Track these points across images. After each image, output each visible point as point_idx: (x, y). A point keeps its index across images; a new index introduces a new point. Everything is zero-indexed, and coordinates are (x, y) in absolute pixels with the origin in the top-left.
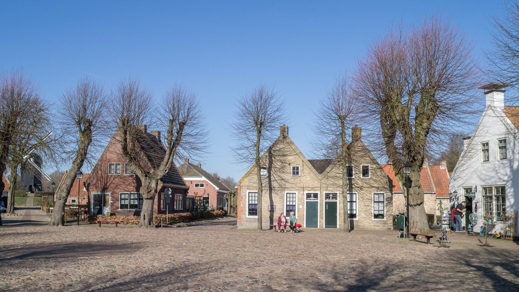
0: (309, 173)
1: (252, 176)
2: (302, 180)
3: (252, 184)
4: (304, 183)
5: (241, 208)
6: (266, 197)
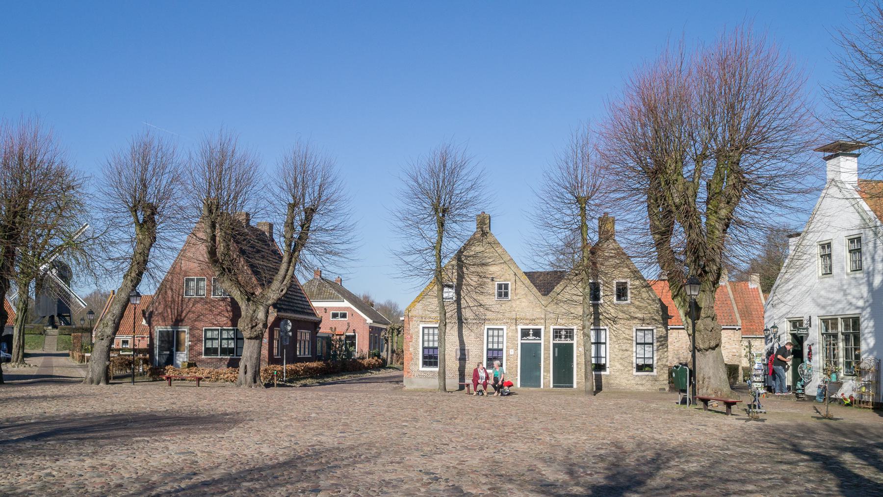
0: (525, 294)
1: (429, 300)
2: (514, 306)
3: (428, 312)
4: (518, 311)
5: (411, 354)
6: (453, 335)
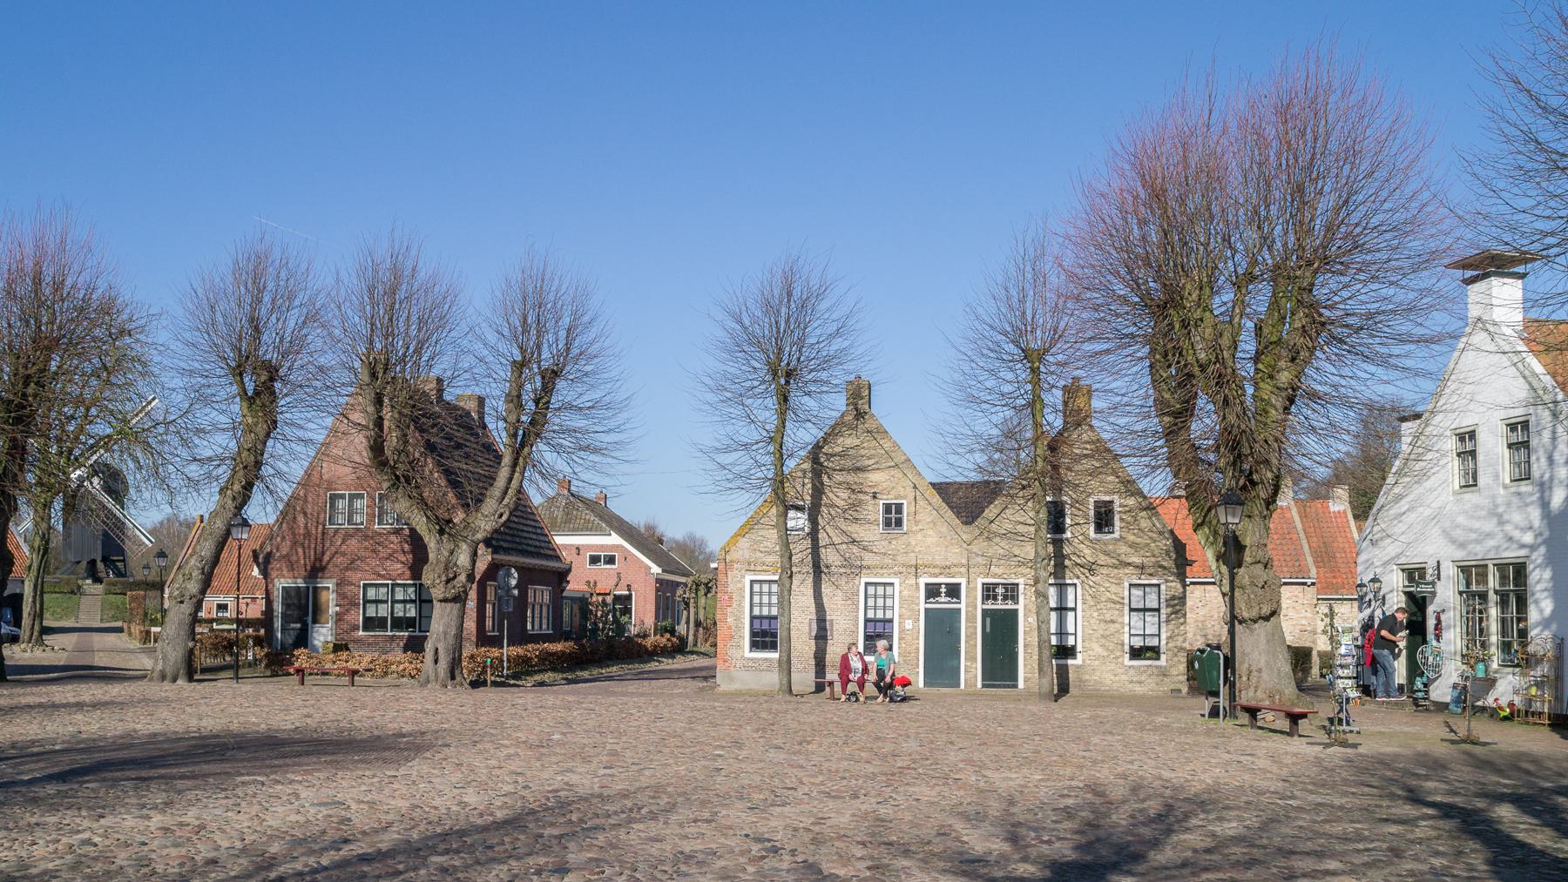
0: (932, 521)
1: (762, 533)
2: (913, 543)
3: (760, 554)
4: (920, 551)
5: (729, 628)
6: (804, 595)
